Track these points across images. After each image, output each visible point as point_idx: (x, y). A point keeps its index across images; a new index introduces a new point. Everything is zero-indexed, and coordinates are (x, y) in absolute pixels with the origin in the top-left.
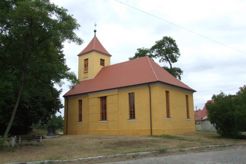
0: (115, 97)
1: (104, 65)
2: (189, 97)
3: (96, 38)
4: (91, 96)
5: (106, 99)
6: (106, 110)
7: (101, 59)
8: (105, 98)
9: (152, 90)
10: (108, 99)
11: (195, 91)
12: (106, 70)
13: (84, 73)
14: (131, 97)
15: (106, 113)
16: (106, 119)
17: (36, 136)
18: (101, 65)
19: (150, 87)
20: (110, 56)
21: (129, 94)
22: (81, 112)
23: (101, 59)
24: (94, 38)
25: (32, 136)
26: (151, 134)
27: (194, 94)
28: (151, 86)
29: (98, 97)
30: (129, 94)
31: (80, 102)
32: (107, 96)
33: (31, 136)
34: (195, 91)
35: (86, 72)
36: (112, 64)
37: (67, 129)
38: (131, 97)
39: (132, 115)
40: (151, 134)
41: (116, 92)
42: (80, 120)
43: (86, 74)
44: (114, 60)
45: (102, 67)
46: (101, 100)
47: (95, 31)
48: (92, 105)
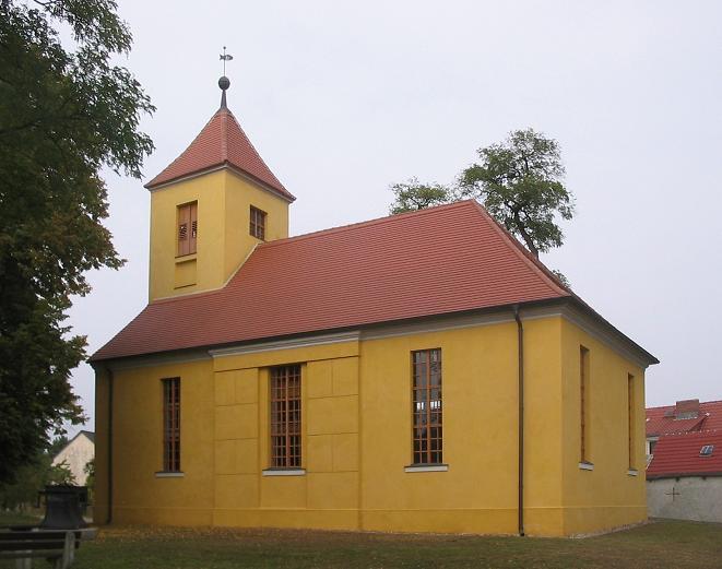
0: (347, 369)
1: (263, 239)
2: (636, 380)
3: (230, 115)
4: (222, 360)
5: (298, 379)
6: (299, 425)
7: (253, 209)
8: (291, 373)
9: (529, 337)
10: (307, 374)
11: (655, 361)
12: (273, 257)
13: (178, 264)
14: (426, 374)
15: (297, 439)
16: (296, 462)
17: (36, 530)
18: (252, 233)
19: (520, 325)
20: (290, 199)
21: (414, 353)
22: (179, 431)
23: (253, 209)
24: (217, 116)
25: (13, 528)
26: (521, 527)
27: (650, 370)
28: (526, 321)
29: (260, 368)
30: (414, 353)
31: (172, 388)
32: (305, 363)
33: (7, 531)
34: (655, 361)
35: (185, 262)
36: (291, 236)
37: (110, 503)
38: (426, 374)
39: (427, 447)
40: (521, 527)
41: (349, 344)
42: (173, 461)
43: (188, 270)
44: (302, 220)
45: (257, 243)
46: (272, 384)
47: (224, 84)
48: (229, 397)
